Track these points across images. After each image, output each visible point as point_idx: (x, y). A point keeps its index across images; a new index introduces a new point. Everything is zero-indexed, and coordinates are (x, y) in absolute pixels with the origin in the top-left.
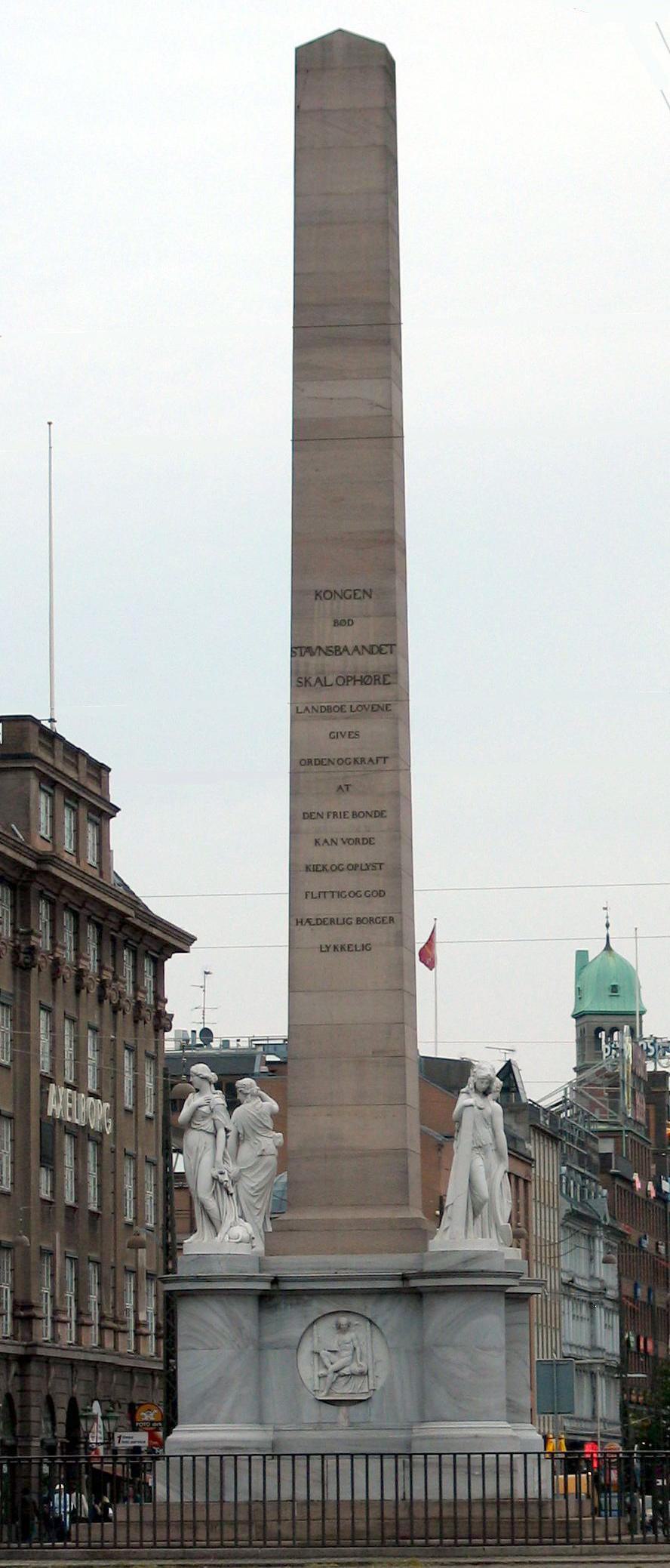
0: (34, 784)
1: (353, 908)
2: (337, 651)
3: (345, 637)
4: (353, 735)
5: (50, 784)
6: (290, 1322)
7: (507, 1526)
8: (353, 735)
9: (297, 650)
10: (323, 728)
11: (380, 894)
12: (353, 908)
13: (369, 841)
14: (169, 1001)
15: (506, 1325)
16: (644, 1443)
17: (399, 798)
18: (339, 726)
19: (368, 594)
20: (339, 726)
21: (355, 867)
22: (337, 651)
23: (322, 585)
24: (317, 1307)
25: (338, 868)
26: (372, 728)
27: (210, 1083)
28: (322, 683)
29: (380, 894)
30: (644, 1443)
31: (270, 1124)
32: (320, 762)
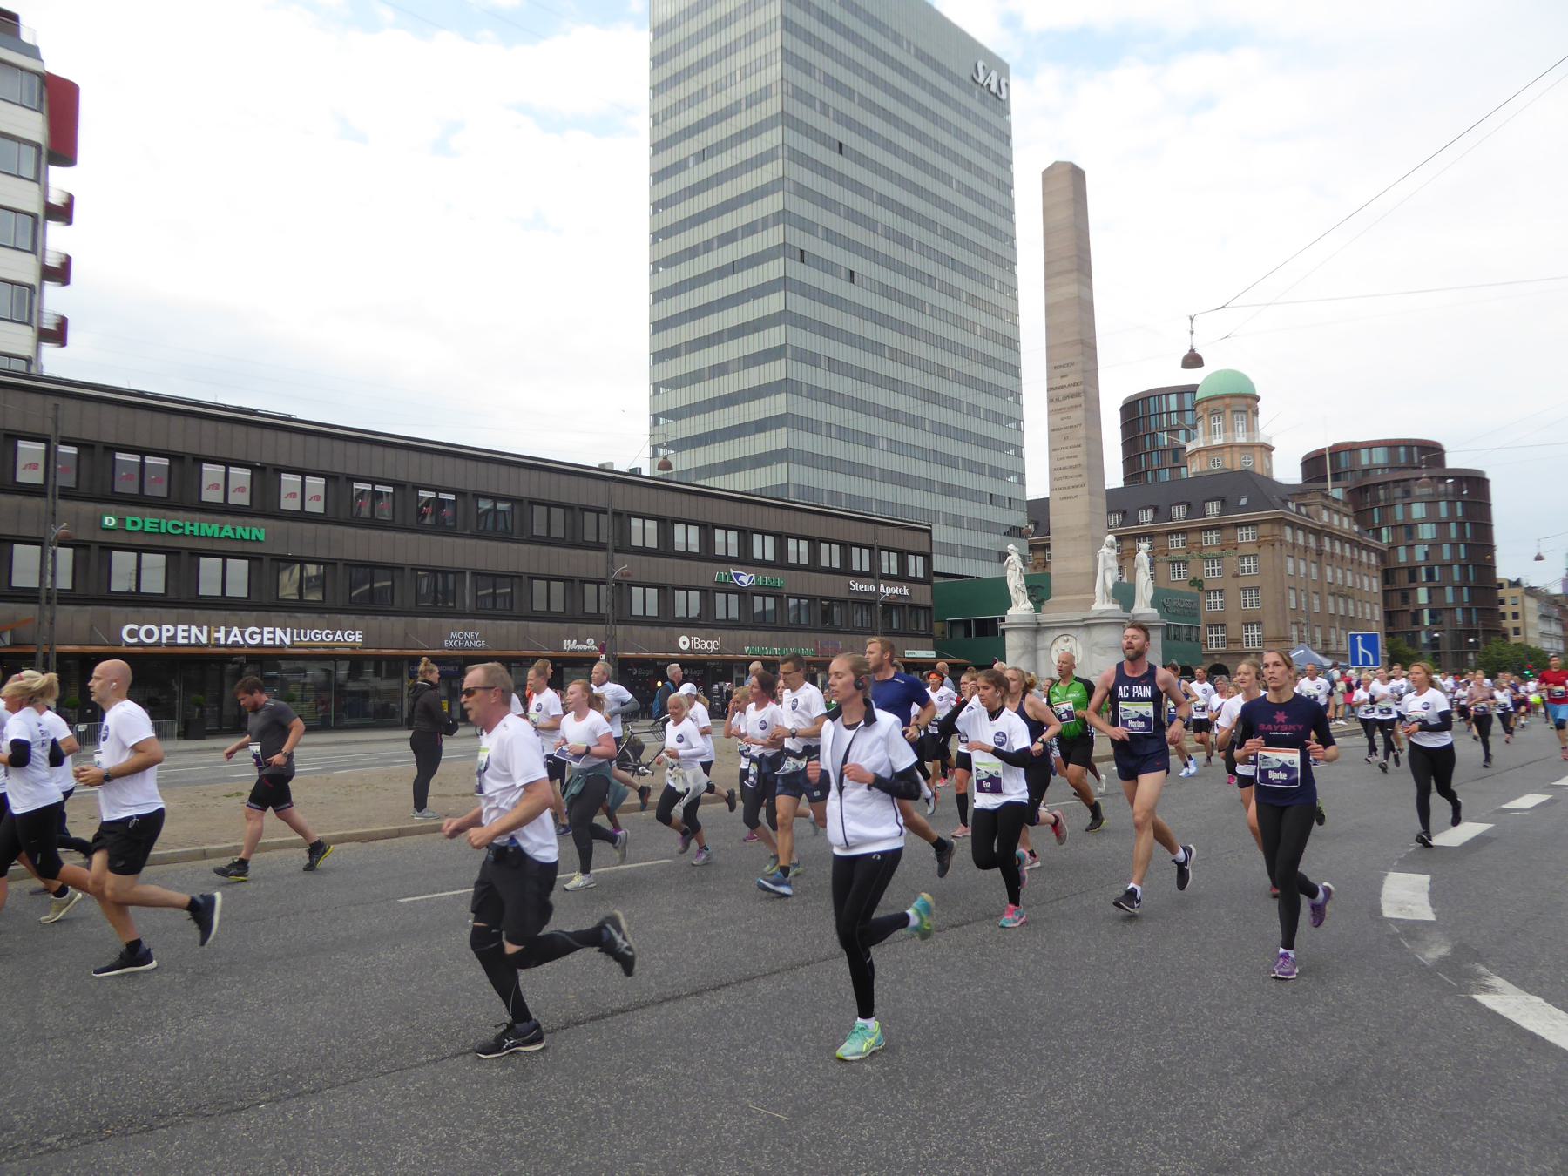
0: (1321, 508)
1: (1071, 482)
2: (1062, 387)
3: (1065, 382)
4: (1069, 418)
5: (1326, 508)
6: (1048, 637)
7: (1237, 456)
8: (1069, 418)
9: (1050, 389)
10: (1059, 416)
11: (1080, 476)
12: (1071, 482)
13: (1075, 457)
14: (63, 349)
15: (820, 736)
16: (89, 711)
17: (1049, 359)
18: (1064, 415)
19: (1072, 364)
20: (1064, 415)
21: (1071, 467)
22: (1062, 387)
23: (1057, 364)
24: (1058, 633)
25: (1065, 468)
26: (1058, 382)
27: (472, 795)
28: (1058, 400)
29: (1080, 476)
30: (89, 711)
31: (961, 792)
32: (1058, 429)
